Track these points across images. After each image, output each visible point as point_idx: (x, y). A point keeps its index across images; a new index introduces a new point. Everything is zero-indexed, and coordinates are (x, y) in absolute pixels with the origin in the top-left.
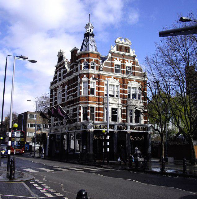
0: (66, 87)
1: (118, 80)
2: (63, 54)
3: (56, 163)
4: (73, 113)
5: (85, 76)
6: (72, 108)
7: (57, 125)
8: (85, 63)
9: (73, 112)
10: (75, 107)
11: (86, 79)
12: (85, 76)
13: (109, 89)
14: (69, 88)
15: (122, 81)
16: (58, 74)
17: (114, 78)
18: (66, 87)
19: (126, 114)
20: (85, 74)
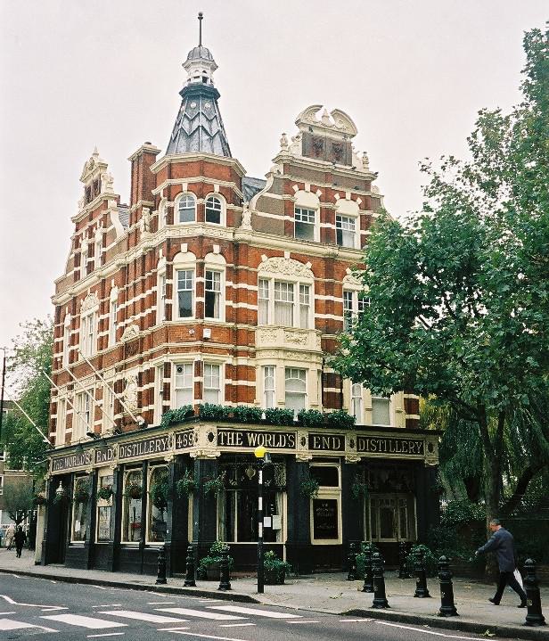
1: (309, 265)
12: (184, 247)
14: (124, 297)
17: (293, 257)
20: (184, 240)
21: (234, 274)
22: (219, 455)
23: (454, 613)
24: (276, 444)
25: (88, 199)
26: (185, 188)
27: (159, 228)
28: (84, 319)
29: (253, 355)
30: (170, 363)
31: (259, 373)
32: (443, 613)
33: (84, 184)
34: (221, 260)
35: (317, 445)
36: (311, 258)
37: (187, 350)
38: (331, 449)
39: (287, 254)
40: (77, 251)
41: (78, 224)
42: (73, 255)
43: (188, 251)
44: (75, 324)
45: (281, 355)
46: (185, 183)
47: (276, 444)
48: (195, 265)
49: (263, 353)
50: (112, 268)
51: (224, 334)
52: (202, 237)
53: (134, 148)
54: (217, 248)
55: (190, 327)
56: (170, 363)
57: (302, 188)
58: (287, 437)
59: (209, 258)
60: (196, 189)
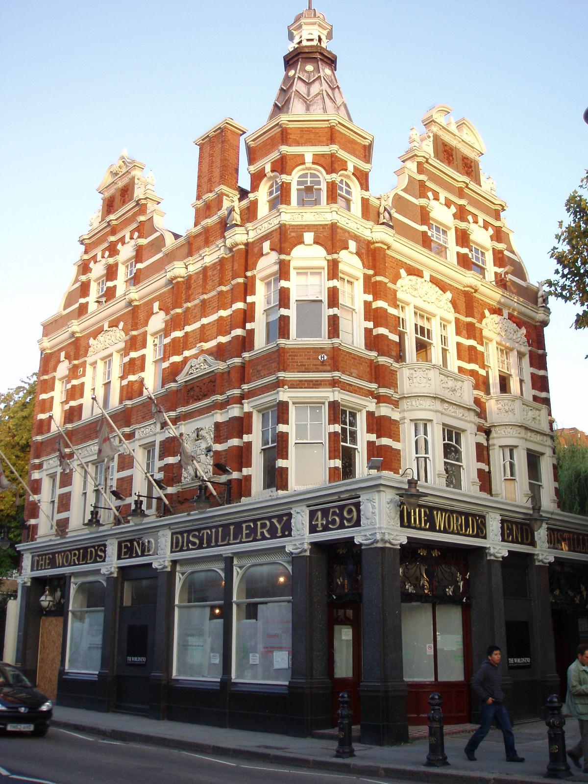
0: (157, 321)
1: (449, 295)
2: (136, 173)
3: (62, 414)
4: (218, 447)
5: (309, 237)
6: (207, 423)
7: (333, 193)
8: (305, 175)
9: (218, 439)
10: (235, 411)
11: (177, 434)
12: (309, 237)
13: (44, 599)
14: (173, 324)
15: (462, 305)
16: (98, 270)
17: (434, 281)
18: (157, 321)
19: (232, 528)
20: (309, 228)
21: (371, 287)
22: (405, 541)
23: (444, 762)
24: (466, 530)
25: (110, 206)
26: (309, 158)
27: (259, 216)
28: (94, 364)
29: (396, 404)
30: (287, 403)
31: (408, 432)
32: (430, 763)
33: (102, 196)
34: (357, 262)
35: (508, 537)
36: (453, 289)
37: (315, 384)
38: (522, 543)
39: (427, 275)
40: (83, 278)
41: (86, 245)
42: (78, 284)
43: (315, 243)
44: (74, 372)
45: (438, 405)
46: (309, 152)
47: (466, 530)
48: (325, 264)
49: (415, 403)
50: (156, 284)
51: (364, 368)
52: (333, 227)
53: (207, 126)
54: (352, 245)
55: (321, 350)
56: (287, 403)
57: (436, 198)
58: (477, 521)
59: (343, 255)
60: (322, 161)
